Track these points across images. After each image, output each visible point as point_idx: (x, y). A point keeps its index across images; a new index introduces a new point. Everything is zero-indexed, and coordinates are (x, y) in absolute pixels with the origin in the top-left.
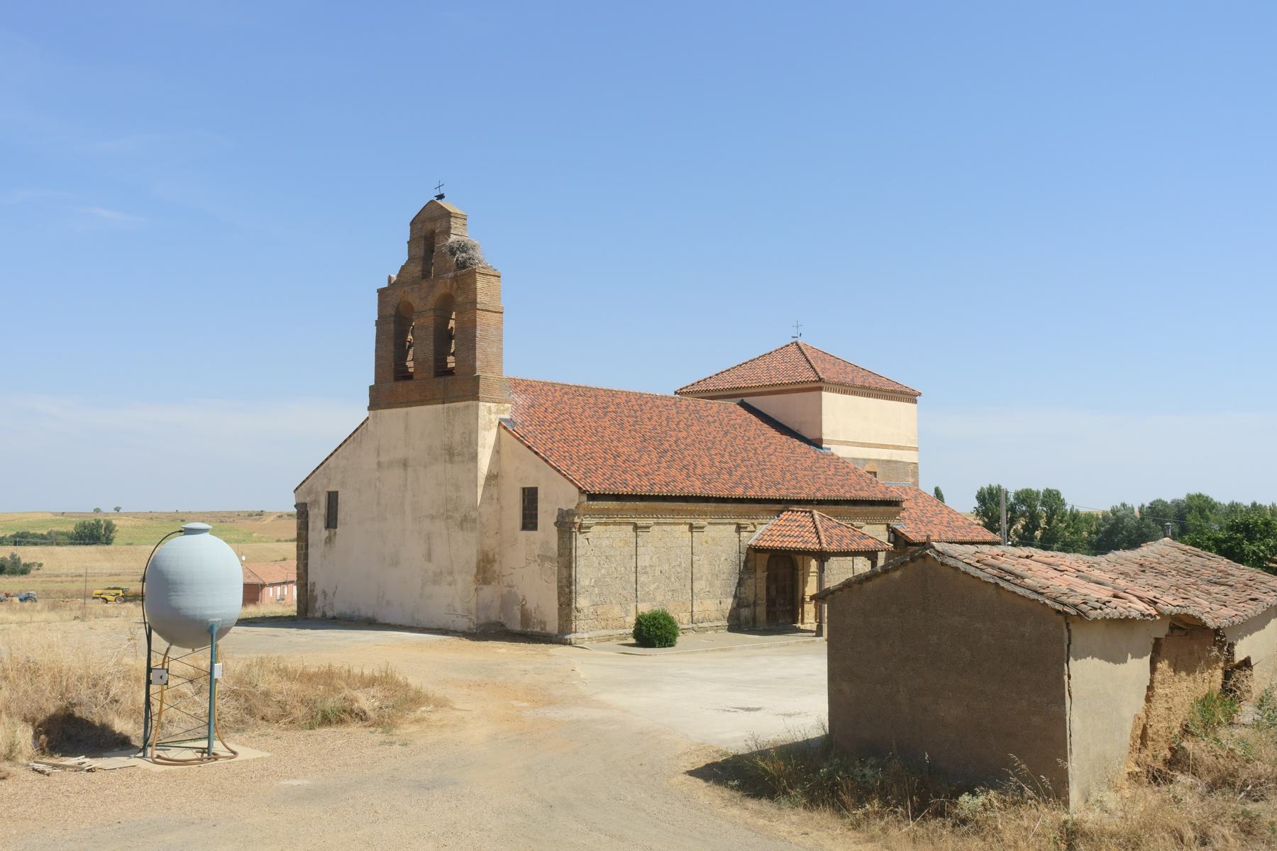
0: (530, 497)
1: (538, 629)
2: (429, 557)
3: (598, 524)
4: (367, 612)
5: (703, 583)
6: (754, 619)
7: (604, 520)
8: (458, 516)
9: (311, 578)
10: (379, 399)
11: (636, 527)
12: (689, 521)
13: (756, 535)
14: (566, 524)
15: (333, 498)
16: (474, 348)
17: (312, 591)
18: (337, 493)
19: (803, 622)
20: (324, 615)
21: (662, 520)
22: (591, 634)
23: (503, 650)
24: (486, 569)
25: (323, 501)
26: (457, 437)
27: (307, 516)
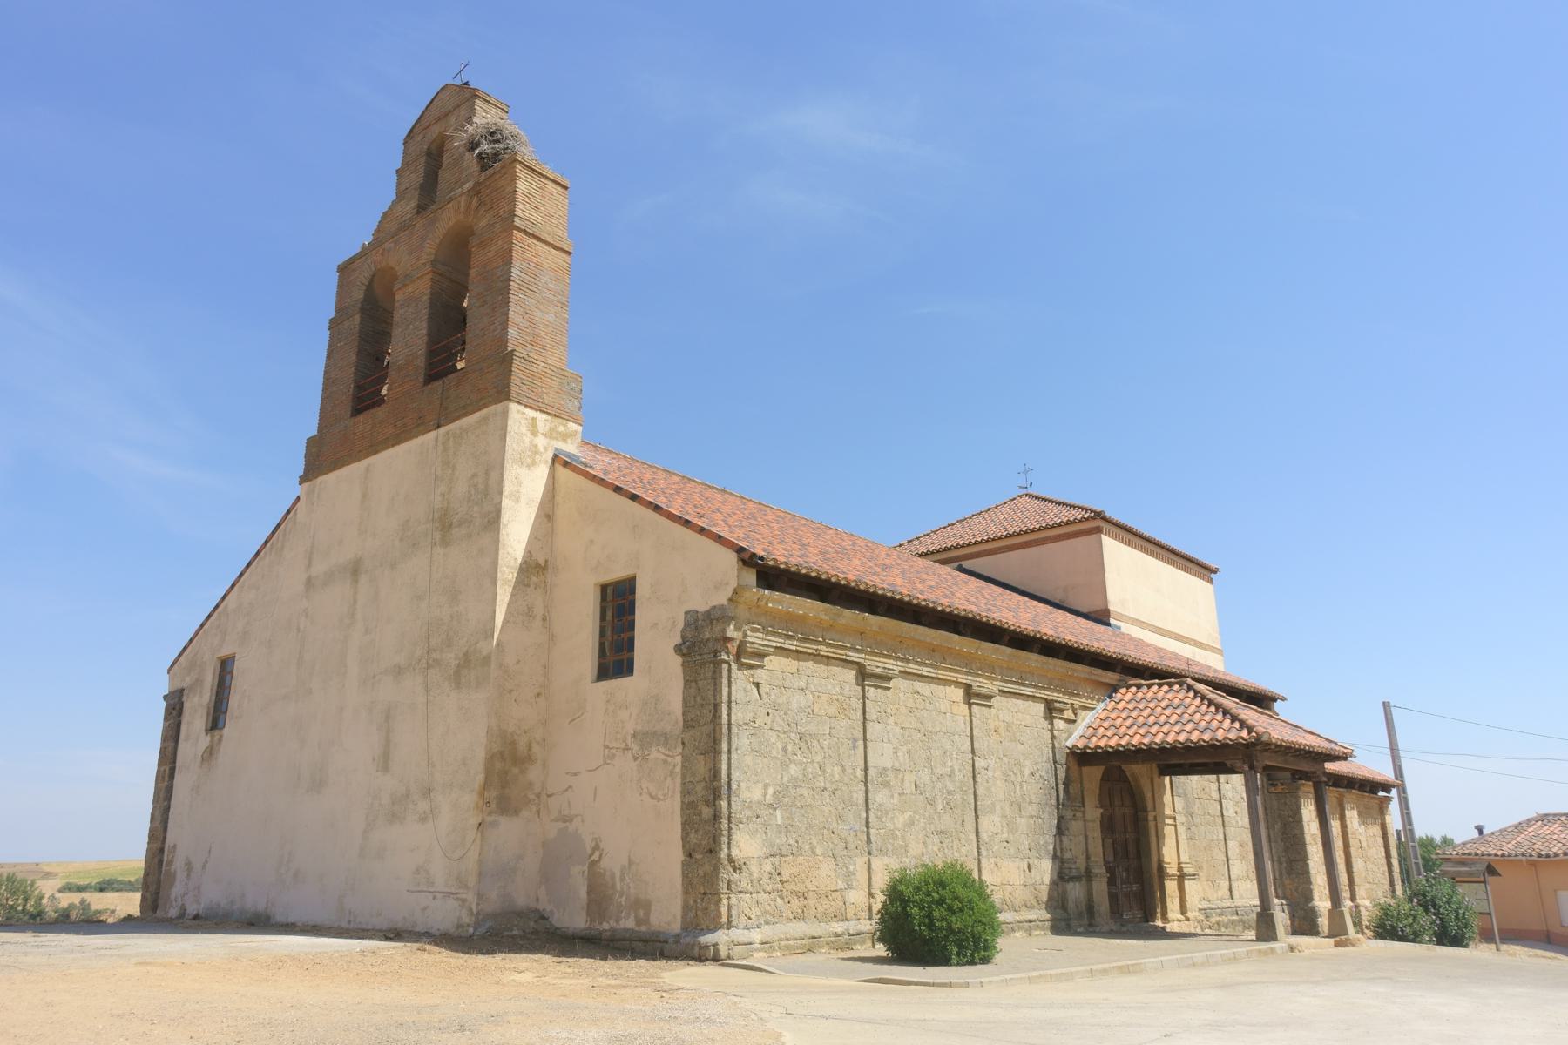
0: (618, 602)
1: (629, 923)
2: (384, 762)
3: (781, 651)
4: (255, 901)
5: (997, 819)
6: (1090, 909)
7: (793, 645)
8: (451, 658)
9: (170, 841)
11: (863, 675)
12: (968, 679)
13: (1079, 729)
14: (704, 648)
15: (225, 667)
16: (506, 303)
17: (170, 863)
18: (232, 658)
19: (1165, 918)
21: (912, 668)
22: (768, 932)
23: (527, 977)
24: (508, 777)
25: (210, 679)
26: (461, 488)
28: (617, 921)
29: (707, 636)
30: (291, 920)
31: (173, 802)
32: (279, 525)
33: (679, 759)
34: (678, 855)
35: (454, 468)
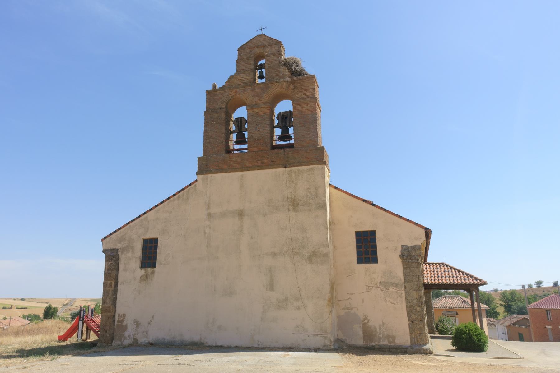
1: (386, 343)
2: (271, 287)
4: (188, 337)
9: (120, 310)
10: (205, 167)
17: (121, 322)
18: (155, 241)
20: (136, 341)
26: (301, 192)
27: (118, 259)
28: (379, 342)
29: (414, 254)
30: (219, 344)
31: (118, 296)
32: (183, 189)
33: (403, 292)
34: (406, 321)
35: (296, 184)
